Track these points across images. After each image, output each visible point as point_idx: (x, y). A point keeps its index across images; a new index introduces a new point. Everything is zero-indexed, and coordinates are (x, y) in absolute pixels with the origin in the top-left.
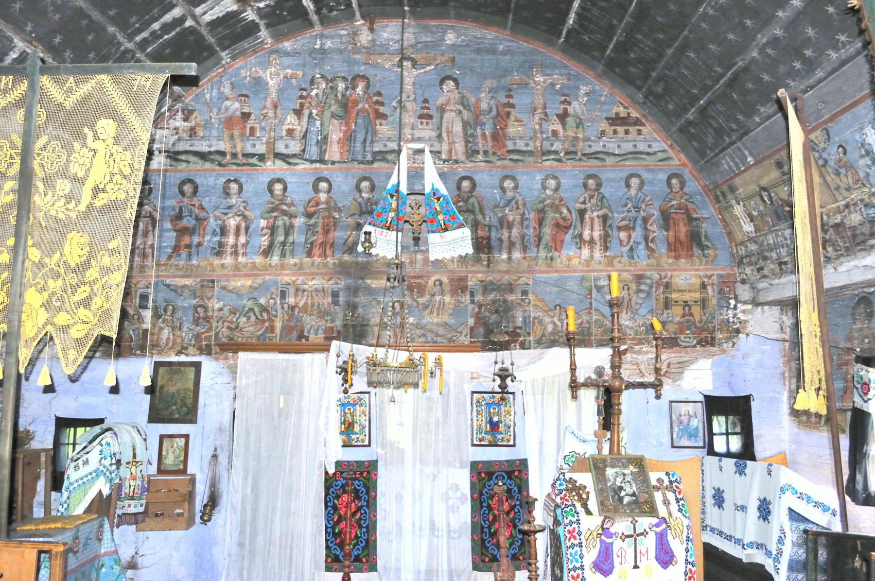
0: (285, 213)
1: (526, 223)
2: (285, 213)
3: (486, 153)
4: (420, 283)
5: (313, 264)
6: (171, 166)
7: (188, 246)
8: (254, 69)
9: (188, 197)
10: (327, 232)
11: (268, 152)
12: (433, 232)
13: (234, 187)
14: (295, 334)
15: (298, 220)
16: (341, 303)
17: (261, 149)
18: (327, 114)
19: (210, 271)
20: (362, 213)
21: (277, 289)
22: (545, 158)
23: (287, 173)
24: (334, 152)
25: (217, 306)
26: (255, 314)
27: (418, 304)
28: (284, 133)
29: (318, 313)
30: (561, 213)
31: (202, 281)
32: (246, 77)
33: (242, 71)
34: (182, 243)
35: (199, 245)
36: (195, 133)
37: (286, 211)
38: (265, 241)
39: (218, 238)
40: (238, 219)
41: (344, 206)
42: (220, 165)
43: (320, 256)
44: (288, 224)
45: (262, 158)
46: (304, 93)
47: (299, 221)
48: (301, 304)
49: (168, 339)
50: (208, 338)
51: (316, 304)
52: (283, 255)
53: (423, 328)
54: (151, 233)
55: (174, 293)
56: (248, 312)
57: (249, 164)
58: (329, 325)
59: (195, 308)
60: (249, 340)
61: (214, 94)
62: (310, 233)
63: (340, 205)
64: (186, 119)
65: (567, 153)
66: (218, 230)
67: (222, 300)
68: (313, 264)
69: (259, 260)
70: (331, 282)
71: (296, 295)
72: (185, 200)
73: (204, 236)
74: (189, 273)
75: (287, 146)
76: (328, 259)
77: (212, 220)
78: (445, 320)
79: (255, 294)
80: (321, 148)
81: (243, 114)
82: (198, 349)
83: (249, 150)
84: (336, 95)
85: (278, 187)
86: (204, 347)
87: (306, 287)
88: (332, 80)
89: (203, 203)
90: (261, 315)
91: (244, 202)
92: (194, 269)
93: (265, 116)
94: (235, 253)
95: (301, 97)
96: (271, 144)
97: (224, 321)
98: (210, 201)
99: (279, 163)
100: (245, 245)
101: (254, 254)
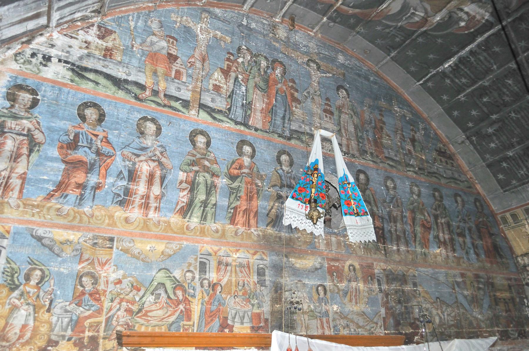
0: (206, 169)
1: (405, 219)
2: (206, 169)
3: (372, 154)
4: (338, 267)
5: (236, 233)
6: (72, 81)
7: (81, 186)
8: (185, 18)
9: (89, 124)
10: (250, 199)
11: (194, 101)
12: (351, 214)
13: (151, 127)
14: (216, 324)
15: (220, 180)
16: (267, 283)
17: (186, 95)
18: (251, 83)
19: (109, 225)
20: (282, 186)
21: (196, 259)
22: (408, 169)
23: (211, 127)
24: (257, 119)
25: (113, 277)
26: (166, 292)
27: (338, 289)
28: (211, 87)
29: (244, 294)
30: (424, 216)
31: (95, 237)
32: (176, 22)
33: (173, 15)
34: (73, 180)
35: (97, 187)
36: (111, 55)
37: (208, 167)
38: (183, 197)
39: (125, 183)
40: (153, 164)
41: (266, 175)
42: (136, 98)
43: (244, 225)
44: (209, 182)
45: (186, 104)
46: (232, 58)
47: (222, 182)
48: (223, 283)
49: (24, 326)
50: (95, 327)
51: (241, 283)
52: (204, 218)
53: (345, 318)
54: (24, 158)
55: (47, 251)
56: (156, 289)
57: (170, 107)
58: (256, 311)
59: (80, 277)
60: (157, 330)
61: (139, 24)
62: (233, 196)
63: (262, 173)
64: (102, 37)
65: (419, 169)
66: (126, 174)
67: (122, 268)
68: (236, 233)
69: (175, 219)
70: (256, 257)
71: (218, 270)
72: (85, 126)
73: (105, 177)
74: (75, 223)
75: (213, 100)
76: (252, 230)
77: (118, 159)
78: (363, 309)
79: (168, 264)
80: (246, 112)
81: (170, 55)
82: (75, 345)
83: (173, 91)
84: (259, 70)
85: (201, 140)
86: (86, 341)
87: (230, 260)
88: (256, 56)
89: (110, 136)
90: (175, 294)
91: (161, 146)
92: (85, 219)
93: (192, 65)
94: (146, 206)
95: (228, 59)
96: (199, 93)
97: (122, 300)
98: (119, 135)
99: (203, 115)
100: (159, 198)
101: (170, 211)
